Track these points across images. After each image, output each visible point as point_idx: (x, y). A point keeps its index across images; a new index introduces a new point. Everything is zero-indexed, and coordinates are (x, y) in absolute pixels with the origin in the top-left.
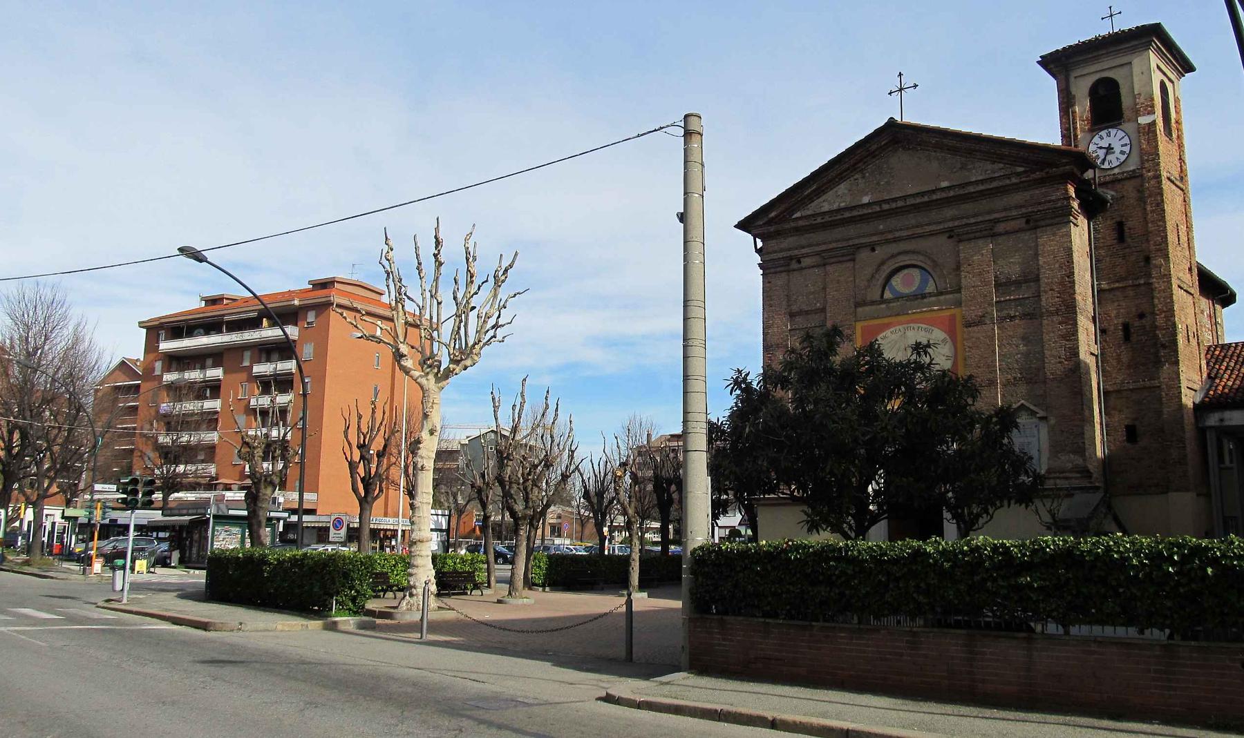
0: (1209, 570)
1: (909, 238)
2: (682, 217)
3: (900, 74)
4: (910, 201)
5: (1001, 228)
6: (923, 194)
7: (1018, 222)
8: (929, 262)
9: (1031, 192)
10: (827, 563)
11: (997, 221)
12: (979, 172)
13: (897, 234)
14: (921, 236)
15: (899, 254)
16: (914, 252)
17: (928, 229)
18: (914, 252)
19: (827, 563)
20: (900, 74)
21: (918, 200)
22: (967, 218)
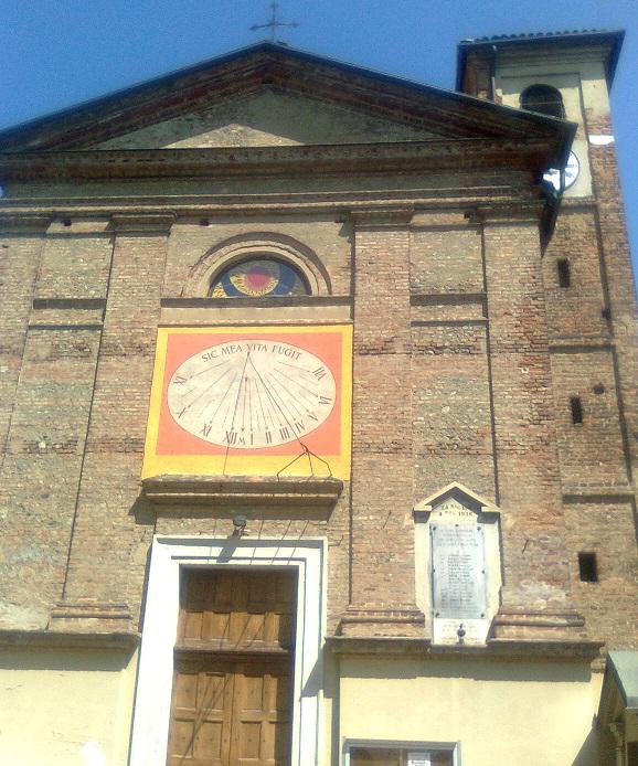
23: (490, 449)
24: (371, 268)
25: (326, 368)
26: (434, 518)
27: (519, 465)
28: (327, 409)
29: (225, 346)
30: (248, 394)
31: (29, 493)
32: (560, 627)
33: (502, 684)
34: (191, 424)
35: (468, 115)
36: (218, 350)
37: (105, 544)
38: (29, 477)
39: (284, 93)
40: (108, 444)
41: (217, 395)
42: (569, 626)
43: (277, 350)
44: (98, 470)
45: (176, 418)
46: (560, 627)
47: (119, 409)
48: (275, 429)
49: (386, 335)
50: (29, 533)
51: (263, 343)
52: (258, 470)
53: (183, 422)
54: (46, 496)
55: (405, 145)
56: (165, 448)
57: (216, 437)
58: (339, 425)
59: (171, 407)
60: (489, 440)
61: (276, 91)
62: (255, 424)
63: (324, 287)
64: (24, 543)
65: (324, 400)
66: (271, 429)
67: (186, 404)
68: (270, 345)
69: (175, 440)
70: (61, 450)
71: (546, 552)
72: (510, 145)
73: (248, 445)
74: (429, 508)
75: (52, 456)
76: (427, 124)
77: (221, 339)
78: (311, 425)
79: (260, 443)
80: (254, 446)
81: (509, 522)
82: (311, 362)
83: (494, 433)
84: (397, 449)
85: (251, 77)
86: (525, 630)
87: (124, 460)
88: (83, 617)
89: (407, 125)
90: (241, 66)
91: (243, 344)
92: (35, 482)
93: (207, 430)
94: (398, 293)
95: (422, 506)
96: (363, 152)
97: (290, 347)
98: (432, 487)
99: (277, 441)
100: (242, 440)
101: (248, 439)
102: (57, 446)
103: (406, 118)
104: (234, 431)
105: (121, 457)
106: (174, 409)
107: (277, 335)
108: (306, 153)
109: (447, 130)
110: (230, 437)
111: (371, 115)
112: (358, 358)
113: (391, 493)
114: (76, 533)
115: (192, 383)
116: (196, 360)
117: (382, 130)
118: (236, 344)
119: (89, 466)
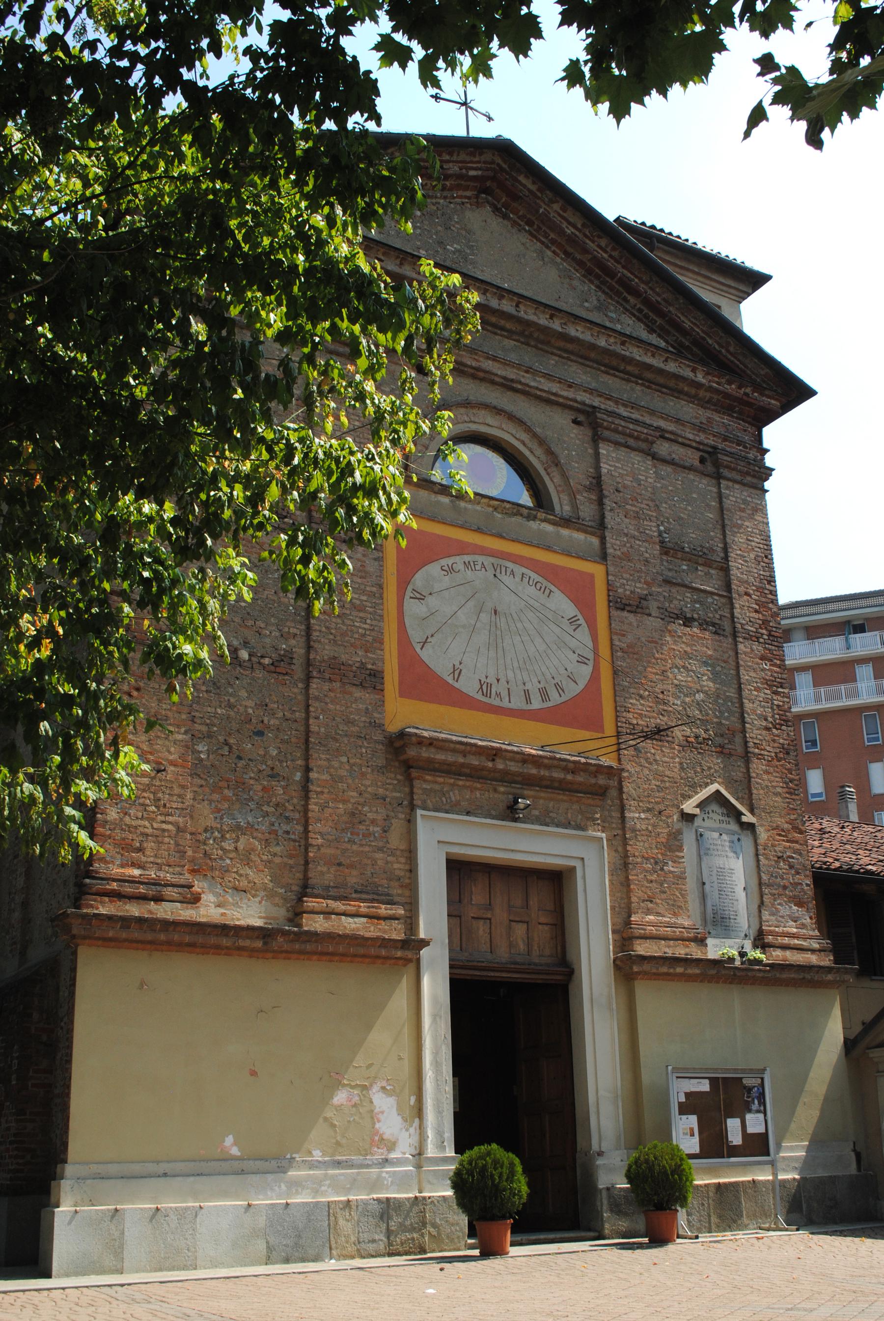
0: (20, 66)
1: (508, 385)
2: (704, 884)
3: (490, 119)
4: (528, 313)
5: (663, 448)
6: (555, 312)
7: (690, 452)
8: (539, 452)
9: (709, 414)
10: (16, 332)
11: (662, 434)
12: (764, 371)
13: (488, 365)
14: (526, 392)
15: (486, 406)
16: (511, 417)
17: (546, 385)
18: (511, 417)
19: (16, 332)
20: (490, 119)
21: (543, 320)
22: (617, 402)
23: (740, 750)
24: (618, 497)
25: (580, 617)
26: (698, 822)
27: (767, 772)
28: (586, 671)
29: (467, 558)
30: (499, 633)
31: (235, 726)
32: (813, 951)
33: (73, 1124)
34: (437, 659)
35: (711, 337)
36: (458, 561)
37: (353, 814)
38: (232, 700)
39: (505, 217)
40: (337, 670)
41: (464, 627)
42: (820, 951)
43: (526, 580)
44: (331, 706)
45: (418, 649)
46: (813, 951)
47: (348, 622)
48: (533, 687)
49: (640, 588)
50: (241, 784)
51: (510, 565)
52: (527, 740)
53: (425, 655)
54: (260, 733)
55: (627, 338)
56: (407, 691)
57: (468, 685)
58: (599, 690)
59: (410, 631)
60: (738, 739)
61: (496, 210)
62: (510, 675)
63: (567, 508)
64: (238, 800)
65: (582, 661)
66: (529, 686)
67: (429, 633)
68: (519, 570)
69: (422, 683)
70: (272, 668)
71: (793, 872)
72: (748, 390)
73: (505, 704)
74: (697, 811)
75: (259, 674)
76: (661, 328)
77: (462, 548)
78: (573, 690)
79: (518, 703)
80: (512, 706)
81: (763, 835)
82: (563, 604)
83: (744, 731)
84: (658, 733)
85: (475, 178)
86: (788, 953)
87: (363, 697)
88: (345, 914)
89: (639, 320)
90: (468, 159)
91: (488, 561)
92: (242, 709)
93: (457, 672)
94: (648, 539)
95: (689, 806)
96: (612, 340)
97: (540, 579)
98: (694, 787)
99: (536, 704)
100: (498, 695)
101: (504, 694)
102: (266, 661)
103: (640, 311)
104: (488, 681)
105: (358, 693)
106: (415, 635)
107: (522, 557)
108: (623, 343)
109: (681, 345)
110: (485, 687)
111: (603, 292)
112: (615, 613)
113: (660, 789)
114: (312, 795)
115: (432, 601)
116: (433, 569)
117: (614, 315)
118: (480, 559)
119: (317, 698)
